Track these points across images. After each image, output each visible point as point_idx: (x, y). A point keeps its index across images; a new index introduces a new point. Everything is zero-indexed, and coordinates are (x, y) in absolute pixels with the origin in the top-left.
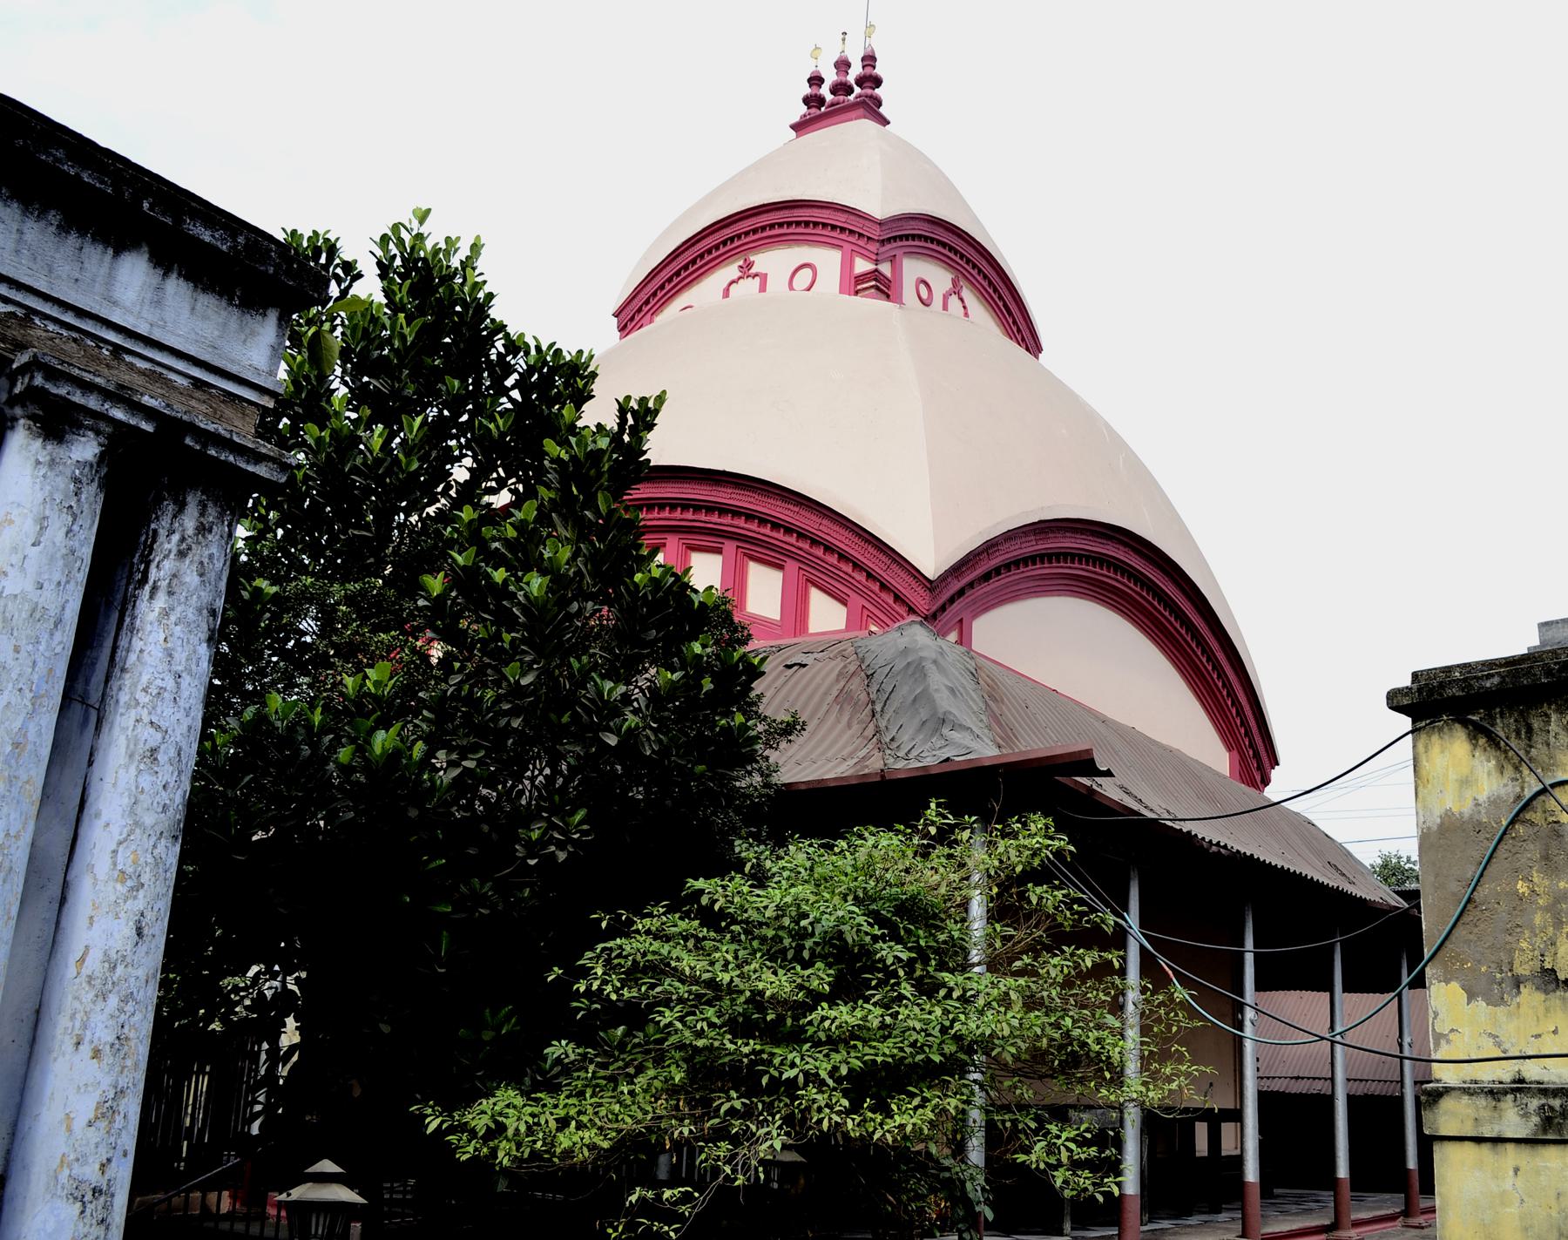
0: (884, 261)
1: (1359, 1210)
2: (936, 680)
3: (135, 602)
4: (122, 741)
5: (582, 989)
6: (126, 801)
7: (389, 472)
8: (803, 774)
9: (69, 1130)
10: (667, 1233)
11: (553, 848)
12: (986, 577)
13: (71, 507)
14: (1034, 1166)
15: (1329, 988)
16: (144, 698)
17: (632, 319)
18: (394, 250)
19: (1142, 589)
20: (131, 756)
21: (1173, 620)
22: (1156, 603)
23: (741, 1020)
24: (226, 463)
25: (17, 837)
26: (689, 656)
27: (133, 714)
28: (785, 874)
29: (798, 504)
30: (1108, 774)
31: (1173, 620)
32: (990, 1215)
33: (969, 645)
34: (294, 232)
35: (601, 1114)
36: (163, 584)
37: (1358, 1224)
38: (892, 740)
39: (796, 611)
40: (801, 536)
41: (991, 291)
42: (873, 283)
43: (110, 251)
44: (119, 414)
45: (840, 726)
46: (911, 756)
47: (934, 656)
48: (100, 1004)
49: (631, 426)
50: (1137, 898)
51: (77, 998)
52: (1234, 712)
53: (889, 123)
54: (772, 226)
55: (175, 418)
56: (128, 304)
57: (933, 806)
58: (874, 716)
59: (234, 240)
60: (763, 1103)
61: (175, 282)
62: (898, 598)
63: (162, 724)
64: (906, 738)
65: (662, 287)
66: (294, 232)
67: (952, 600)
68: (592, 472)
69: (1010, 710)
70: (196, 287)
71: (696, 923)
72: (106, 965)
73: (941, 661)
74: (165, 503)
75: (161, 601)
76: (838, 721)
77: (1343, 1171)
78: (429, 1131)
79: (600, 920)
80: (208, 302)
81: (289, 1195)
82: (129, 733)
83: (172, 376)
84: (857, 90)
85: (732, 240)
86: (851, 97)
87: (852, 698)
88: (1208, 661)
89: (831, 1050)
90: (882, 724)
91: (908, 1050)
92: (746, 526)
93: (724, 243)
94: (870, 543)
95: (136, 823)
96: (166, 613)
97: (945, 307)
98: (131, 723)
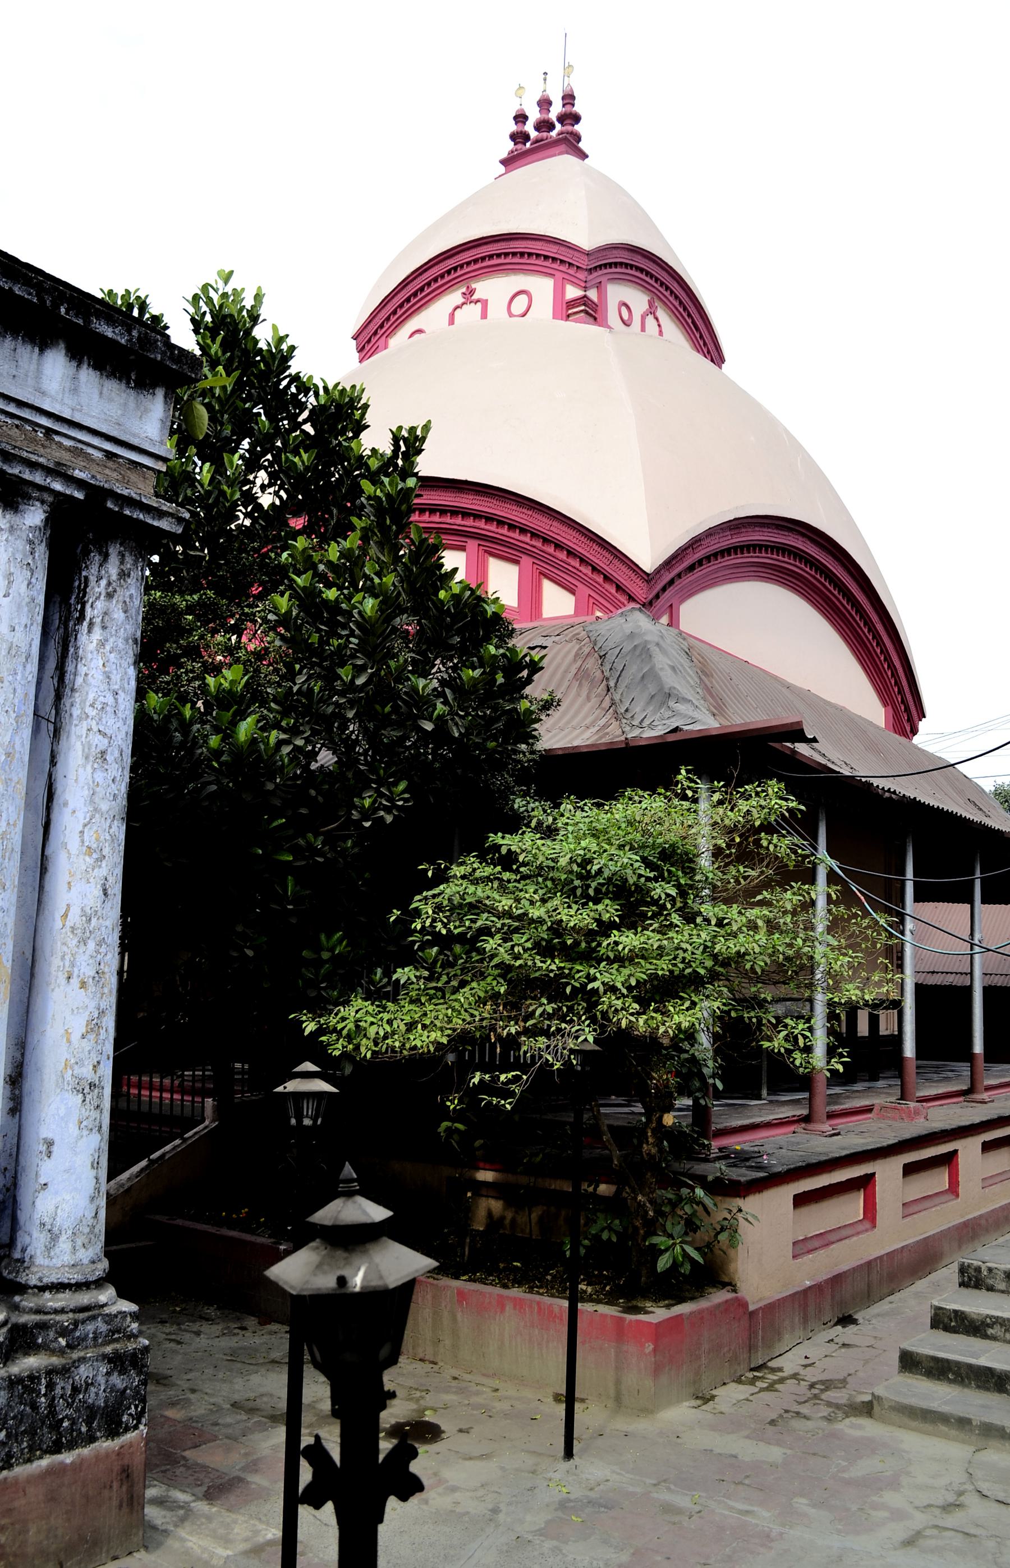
0: (591, 287)
1: (988, 1077)
2: (661, 661)
3: (76, 635)
4: (78, 746)
5: (419, 927)
6: (86, 793)
7: (217, 500)
8: (554, 740)
9: (69, 1041)
10: (504, 1105)
11: (382, 813)
12: (691, 568)
13: (29, 564)
14: (776, 1051)
15: (971, 901)
16: (92, 712)
17: (369, 341)
18: (204, 308)
19: (816, 572)
20: (87, 758)
21: (841, 597)
22: (827, 584)
23: (544, 943)
24: (137, 520)
25: (15, 825)
26: (486, 656)
27: (85, 725)
28: (570, 828)
29: (531, 508)
30: (814, 740)
31: (841, 597)
32: (720, 1086)
33: (678, 627)
34: (110, 292)
35: (440, 1017)
36: (98, 620)
37: (989, 1088)
38: (627, 710)
39: (531, 598)
40: (534, 535)
41: (681, 310)
42: (583, 308)
43: (37, 349)
44: (58, 486)
45: (580, 700)
46: (644, 725)
47: (656, 639)
48: (82, 948)
49: (403, 453)
50: (825, 835)
51: (64, 944)
52: (889, 674)
53: (587, 156)
54: (491, 257)
55: (99, 487)
56: (53, 393)
57: (683, 772)
58: (608, 690)
59: (130, 334)
60: (567, 1006)
61: (86, 371)
62: (619, 588)
63: (107, 731)
64: (638, 710)
65: (394, 312)
66: (110, 292)
67: (664, 589)
68: (404, 507)
69: (718, 683)
70: (102, 374)
71: (499, 868)
72: (84, 918)
73: (661, 643)
74: (92, 554)
75: (97, 634)
76: (578, 695)
77: (978, 1048)
78: (306, 1033)
79: (426, 871)
80: (112, 387)
81: (285, 1088)
82: (83, 739)
83: (90, 451)
84: (558, 127)
85: (455, 269)
86: (554, 134)
87: (589, 675)
88: (869, 632)
89: (620, 966)
90: (617, 697)
91: (681, 966)
92: (487, 527)
93: (449, 272)
94: (594, 541)
95: (95, 810)
96: (102, 644)
97: (643, 329)
98: (84, 732)
